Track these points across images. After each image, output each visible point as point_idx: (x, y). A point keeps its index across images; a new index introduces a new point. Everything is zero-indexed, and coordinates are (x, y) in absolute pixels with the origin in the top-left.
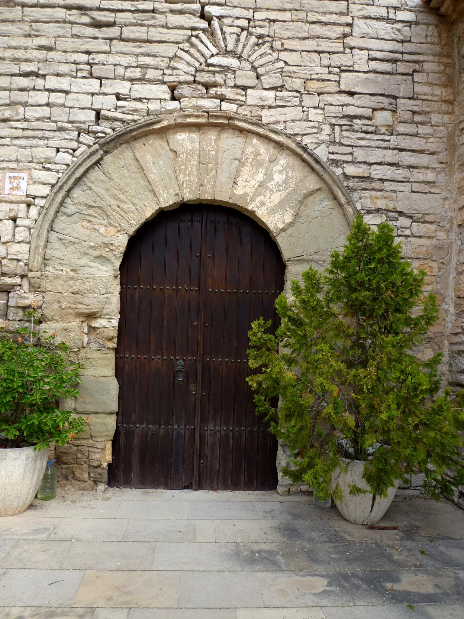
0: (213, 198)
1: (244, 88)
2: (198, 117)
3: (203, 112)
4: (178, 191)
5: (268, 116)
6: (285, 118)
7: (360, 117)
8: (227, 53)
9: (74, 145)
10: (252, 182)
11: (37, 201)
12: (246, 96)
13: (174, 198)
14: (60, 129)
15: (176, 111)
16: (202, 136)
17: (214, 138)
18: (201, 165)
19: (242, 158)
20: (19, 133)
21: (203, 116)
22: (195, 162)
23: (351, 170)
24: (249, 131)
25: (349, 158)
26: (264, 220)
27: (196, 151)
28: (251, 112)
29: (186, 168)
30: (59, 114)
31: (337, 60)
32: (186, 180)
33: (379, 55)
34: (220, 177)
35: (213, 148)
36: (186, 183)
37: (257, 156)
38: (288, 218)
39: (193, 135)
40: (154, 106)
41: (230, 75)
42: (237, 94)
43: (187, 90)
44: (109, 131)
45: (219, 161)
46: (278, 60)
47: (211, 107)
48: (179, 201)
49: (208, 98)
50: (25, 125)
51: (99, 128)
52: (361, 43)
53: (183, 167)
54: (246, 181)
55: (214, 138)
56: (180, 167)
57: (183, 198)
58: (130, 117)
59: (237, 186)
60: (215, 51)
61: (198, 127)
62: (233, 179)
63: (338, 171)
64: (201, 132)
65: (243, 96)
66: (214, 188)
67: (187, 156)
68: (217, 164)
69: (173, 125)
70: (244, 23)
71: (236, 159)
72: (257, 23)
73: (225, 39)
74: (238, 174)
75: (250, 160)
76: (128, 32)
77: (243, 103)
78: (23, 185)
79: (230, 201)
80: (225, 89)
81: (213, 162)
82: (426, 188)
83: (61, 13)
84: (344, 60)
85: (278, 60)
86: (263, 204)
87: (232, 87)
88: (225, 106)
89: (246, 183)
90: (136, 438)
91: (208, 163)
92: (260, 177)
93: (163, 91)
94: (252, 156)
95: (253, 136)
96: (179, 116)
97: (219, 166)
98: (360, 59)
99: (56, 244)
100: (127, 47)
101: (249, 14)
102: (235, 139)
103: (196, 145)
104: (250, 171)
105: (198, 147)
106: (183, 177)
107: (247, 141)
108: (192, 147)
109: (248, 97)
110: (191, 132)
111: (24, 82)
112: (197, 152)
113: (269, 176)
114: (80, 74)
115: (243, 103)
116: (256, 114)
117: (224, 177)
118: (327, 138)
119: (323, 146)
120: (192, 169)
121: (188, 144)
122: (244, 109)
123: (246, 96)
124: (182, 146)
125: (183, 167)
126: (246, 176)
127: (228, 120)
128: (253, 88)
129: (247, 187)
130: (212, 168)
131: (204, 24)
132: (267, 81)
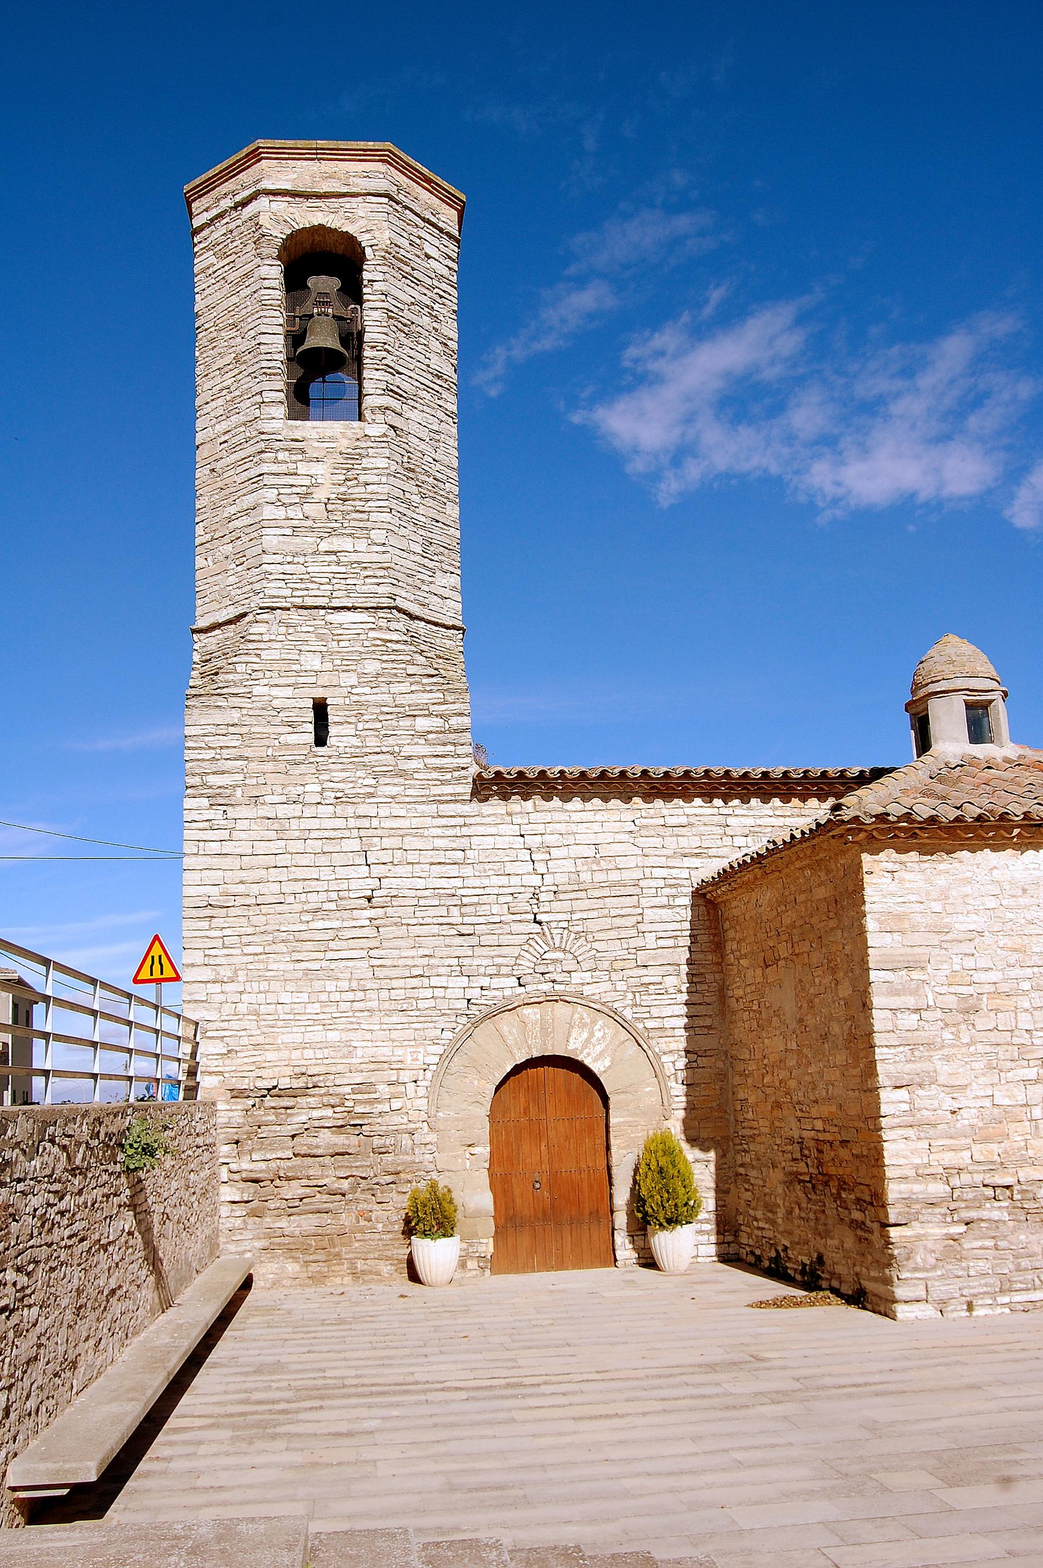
1: (569, 972)
5: (587, 990)
6: (599, 990)
7: (653, 984)
8: (555, 949)
9: (454, 1025)
10: (580, 1040)
11: (431, 1067)
14: (443, 1014)
20: (415, 1019)
23: (650, 1024)
25: (647, 1015)
26: (590, 1066)
30: (443, 1005)
31: (633, 943)
33: (664, 934)
38: (607, 1063)
40: (508, 992)
41: (559, 965)
44: (477, 1013)
46: (592, 949)
50: (418, 1013)
51: (470, 1012)
52: (650, 927)
58: (491, 1002)
60: (547, 949)
63: (640, 1026)
70: (565, 924)
72: (575, 923)
73: (553, 938)
76: (486, 940)
78: (420, 1056)
82: (706, 1031)
83: (436, 929)
84: (639, 942)
85: (592, 949)
86: (589, 1054)
88: (557, 987)
90: (805, 1293)
92: (585, 1035)
93: (513, 981)
98: (650, 940)
99: (445, 1096)
100: (485, 951)
101: (567, 917)
103: (538, 1016)
111: (415, 982)
113: (592, 1034)
114: (453, 974)
118: (630, 1002)
119: (628, 1008)
131: (537, 928)
132: (585, 966)
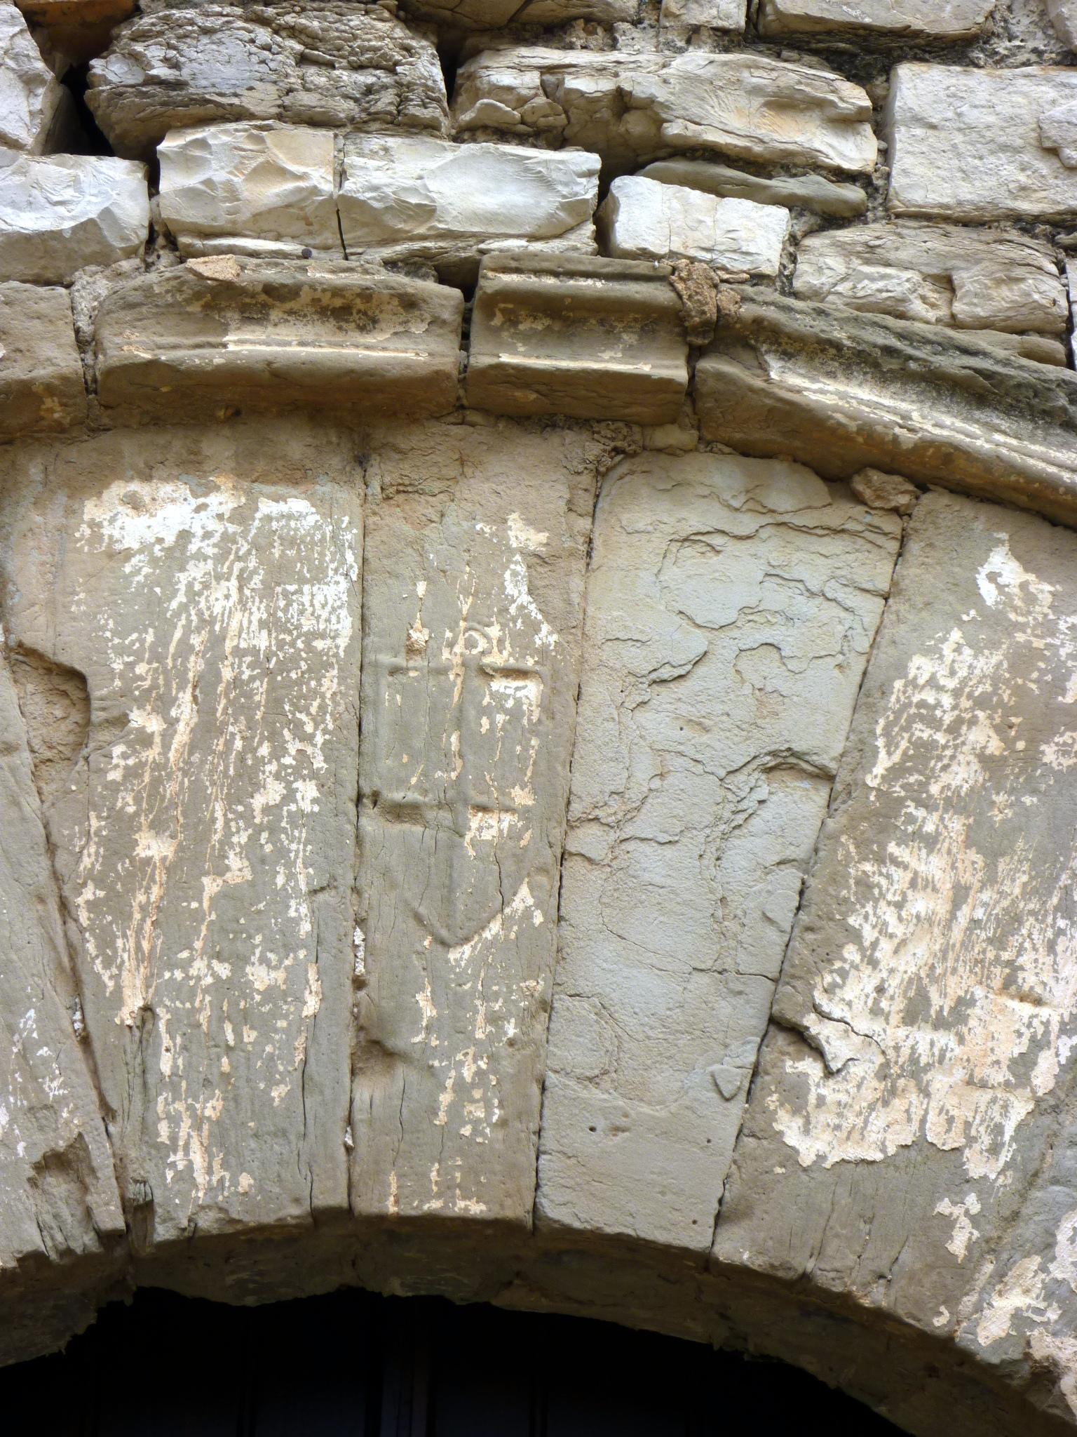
0: (516, 1210)
2: (348, 310)
3: (412, 264)
4: (75, 1121)
10: (1000, 1027)
12: (882, 130)
13: (24, 1200)
15: (104, 258)
16: (394, 520)
17: (523, 535)
18: (372, 823)
19: (862, 752)
21: (409, 303)
22: (308, 791)
24: (938, 475)
27: (319, 665)
28: (946, 283)
29: (196, 856)
32: (185, 991)
34: (603, 967)
35: (522, 641)
36: (185, 1023)
37: (1039, 731)
39: (294, 510)
42: (785, 103)
43: (232, 47)
45: (590, 784)
47: (502, 223)
48: (84, 1241)
49: (462, 135)
53: (154, 847)
54: (915, 1012)
55: (523, 535)
56: (119, 841)
57: (140, 1210)
59: (810, 1067)
61: (347, 420)
62: (760, 992)
64: (382, 473)
65: (846, 123)
66: (530, 1088)
67: (207, 728)
68: (562, 810)
69: (58, 388)
71: (786, 763)
74: (817, 921)
75: (962, 775)
77: (854, 193)
79: (736, 1248)
80: (649, 57)
81: (521, 797)
87: (726, 39)
88: (653, 213)
89: (923, 1039)
91: (456, 803)
94: (982, 736)
95: (979, 519)
96: (131, 306)
97: (589, 840)
102: (771, 550)
103: (327, 606)
104: (960, 895)
105: (346, 625)
106: (155, 962)
107: (911, 572)
108: (271, 624)
109: (901, 136)
110: (262, 470)
112: (330, 684)
115: (854, 193)
116: (1004, 299)
117: (647, 967)
120: (259, 862)
121: (221, 599)
122: (870, 254)
123: (882, 130)
124: (153, 610)
125: (154, 847)
126: (921, 952)
127: (694, 355)
128: (953, 49)
129: (939, 1081)
130: (507, 865)
